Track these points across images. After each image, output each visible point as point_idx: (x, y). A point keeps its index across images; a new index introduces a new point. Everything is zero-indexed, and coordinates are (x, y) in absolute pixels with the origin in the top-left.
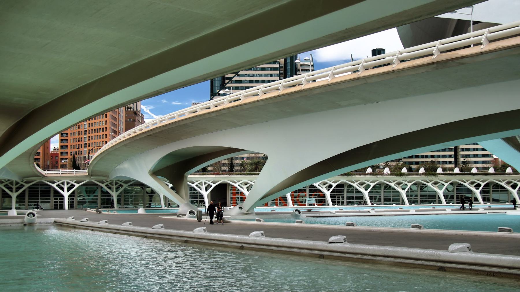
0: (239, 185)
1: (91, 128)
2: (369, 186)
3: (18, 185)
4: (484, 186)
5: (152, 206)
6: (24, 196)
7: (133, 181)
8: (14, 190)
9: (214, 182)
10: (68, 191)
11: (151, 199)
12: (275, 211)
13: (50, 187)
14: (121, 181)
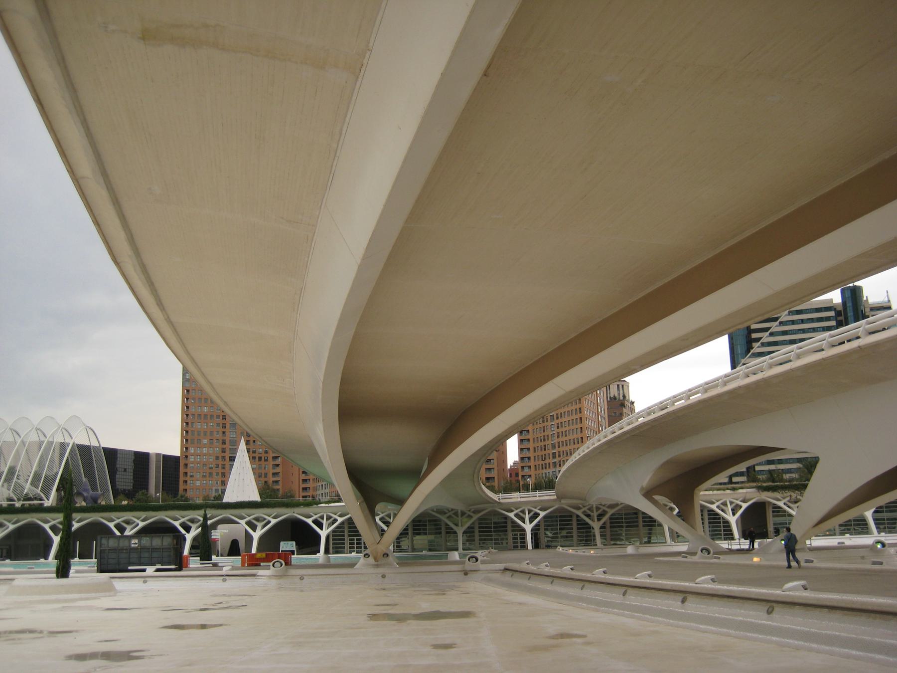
1: (560, 430)
2: (336, 520)
3: (599, 512)
5: (652, 541)
6: (473, 532)
7: (621, 504)
9: (744, 501)
10: (531, 522)
12: (158, 570)
13: (506, 517)
14: (604, 506)
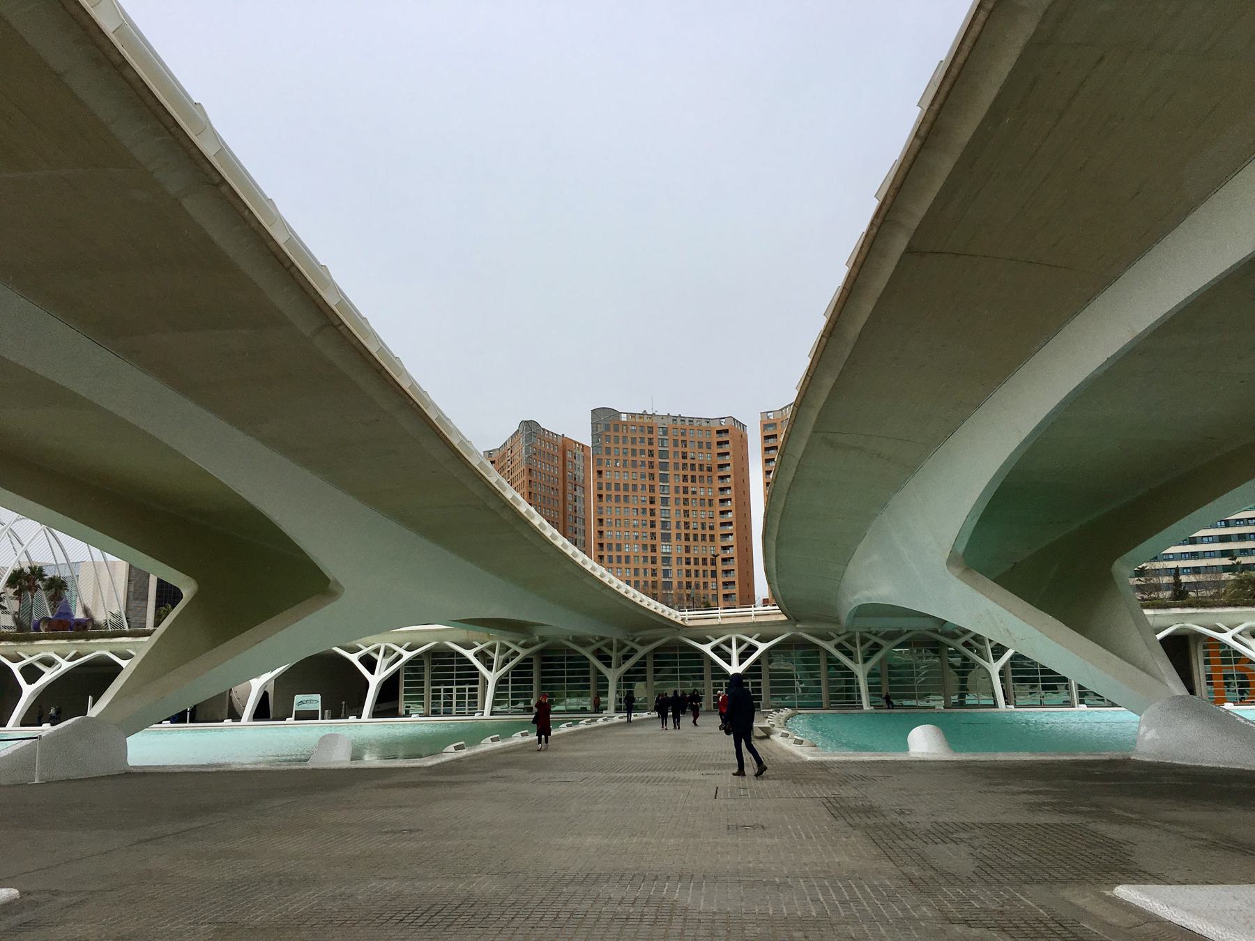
0: (1234, 638)
3: (625, 651)
7: (908, 631)
11: (964, 681)
14: (876, 634)
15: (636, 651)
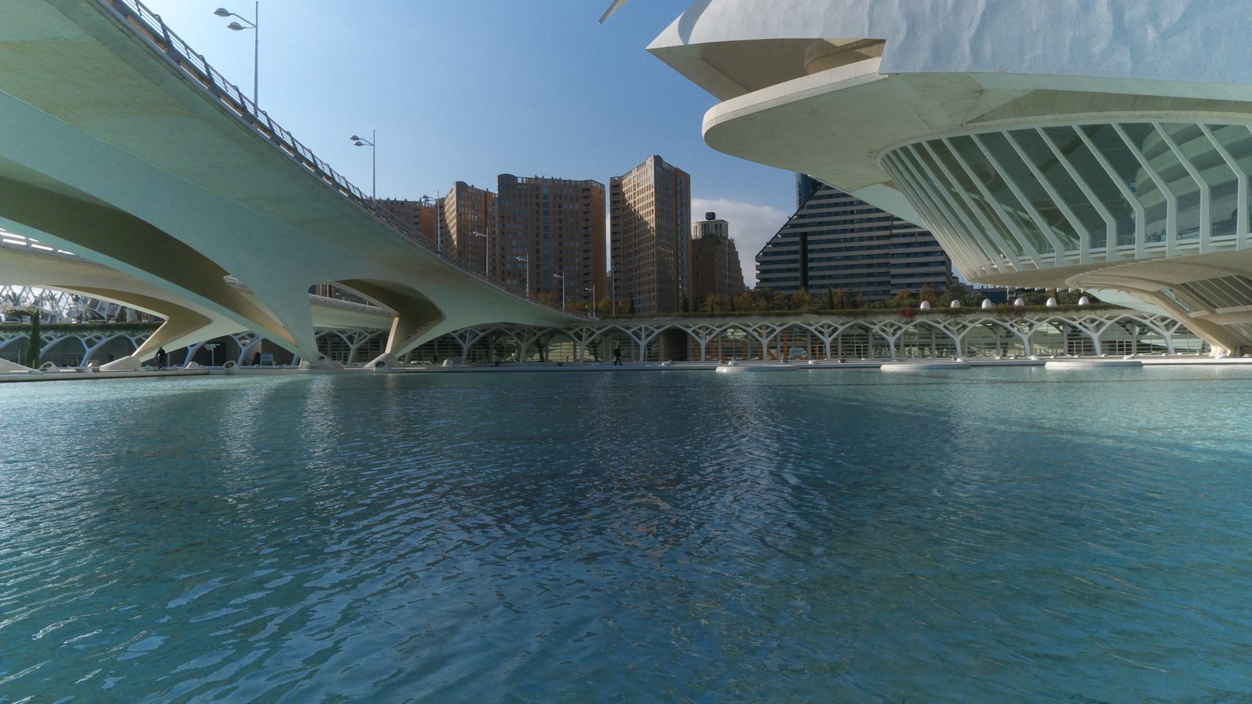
2: (653, 332)
4: (1110, 326)
8: (525, 340)
15: (714, 331)
